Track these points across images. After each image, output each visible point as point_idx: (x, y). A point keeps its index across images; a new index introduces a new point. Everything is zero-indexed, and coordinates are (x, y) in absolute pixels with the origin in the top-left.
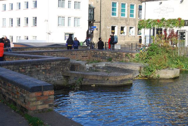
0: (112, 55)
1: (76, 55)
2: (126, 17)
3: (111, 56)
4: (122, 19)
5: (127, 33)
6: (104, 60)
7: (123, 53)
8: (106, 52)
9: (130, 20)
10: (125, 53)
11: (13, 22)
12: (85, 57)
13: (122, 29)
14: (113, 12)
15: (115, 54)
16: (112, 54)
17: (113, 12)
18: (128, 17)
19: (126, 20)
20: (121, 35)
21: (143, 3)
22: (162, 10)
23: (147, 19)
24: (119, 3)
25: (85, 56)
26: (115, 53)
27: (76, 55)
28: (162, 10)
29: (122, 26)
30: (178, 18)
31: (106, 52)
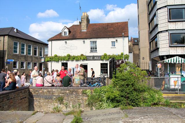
0: (63, 93)
1: (14, 98)
2: (25, 54)
3: (61, 94)
4: (22, 56)
5: (26, 67)
6: (50, 100)
7: (79, 90)
8: (54, 90)
9: (28, 57)
10: (82, 90)
11: (138, 22)
12: (23, 100)
13: (22, 64)
14: (15, 50)
15: (67, 91)
16: (63, 91)
17: (15, 50)
18: (26, 54)
19: (25, 57)
20: (21, 69)
21: (49, 42)
22: (67, 48)
23: (53, 55)
24: (19, 43)
25: (24, 98)
26: (66, 90)
27: (14, 98)
28: (67, 48)
29: (22, 61)
30: (55, 55)
31: (54, 90)
